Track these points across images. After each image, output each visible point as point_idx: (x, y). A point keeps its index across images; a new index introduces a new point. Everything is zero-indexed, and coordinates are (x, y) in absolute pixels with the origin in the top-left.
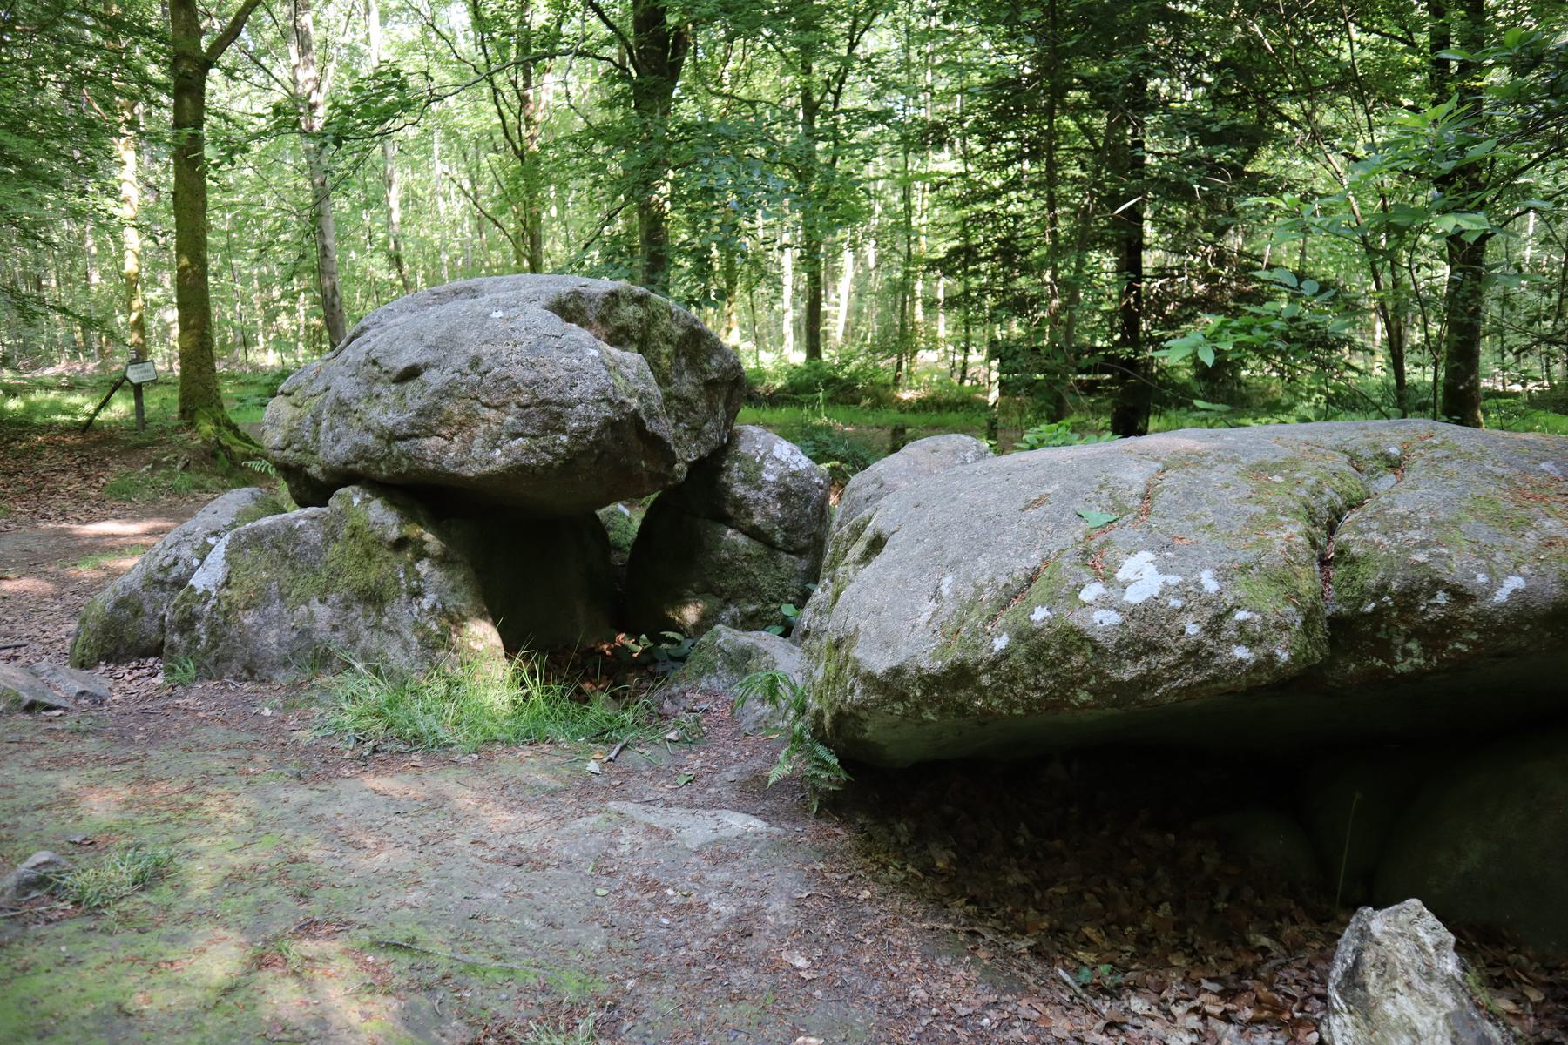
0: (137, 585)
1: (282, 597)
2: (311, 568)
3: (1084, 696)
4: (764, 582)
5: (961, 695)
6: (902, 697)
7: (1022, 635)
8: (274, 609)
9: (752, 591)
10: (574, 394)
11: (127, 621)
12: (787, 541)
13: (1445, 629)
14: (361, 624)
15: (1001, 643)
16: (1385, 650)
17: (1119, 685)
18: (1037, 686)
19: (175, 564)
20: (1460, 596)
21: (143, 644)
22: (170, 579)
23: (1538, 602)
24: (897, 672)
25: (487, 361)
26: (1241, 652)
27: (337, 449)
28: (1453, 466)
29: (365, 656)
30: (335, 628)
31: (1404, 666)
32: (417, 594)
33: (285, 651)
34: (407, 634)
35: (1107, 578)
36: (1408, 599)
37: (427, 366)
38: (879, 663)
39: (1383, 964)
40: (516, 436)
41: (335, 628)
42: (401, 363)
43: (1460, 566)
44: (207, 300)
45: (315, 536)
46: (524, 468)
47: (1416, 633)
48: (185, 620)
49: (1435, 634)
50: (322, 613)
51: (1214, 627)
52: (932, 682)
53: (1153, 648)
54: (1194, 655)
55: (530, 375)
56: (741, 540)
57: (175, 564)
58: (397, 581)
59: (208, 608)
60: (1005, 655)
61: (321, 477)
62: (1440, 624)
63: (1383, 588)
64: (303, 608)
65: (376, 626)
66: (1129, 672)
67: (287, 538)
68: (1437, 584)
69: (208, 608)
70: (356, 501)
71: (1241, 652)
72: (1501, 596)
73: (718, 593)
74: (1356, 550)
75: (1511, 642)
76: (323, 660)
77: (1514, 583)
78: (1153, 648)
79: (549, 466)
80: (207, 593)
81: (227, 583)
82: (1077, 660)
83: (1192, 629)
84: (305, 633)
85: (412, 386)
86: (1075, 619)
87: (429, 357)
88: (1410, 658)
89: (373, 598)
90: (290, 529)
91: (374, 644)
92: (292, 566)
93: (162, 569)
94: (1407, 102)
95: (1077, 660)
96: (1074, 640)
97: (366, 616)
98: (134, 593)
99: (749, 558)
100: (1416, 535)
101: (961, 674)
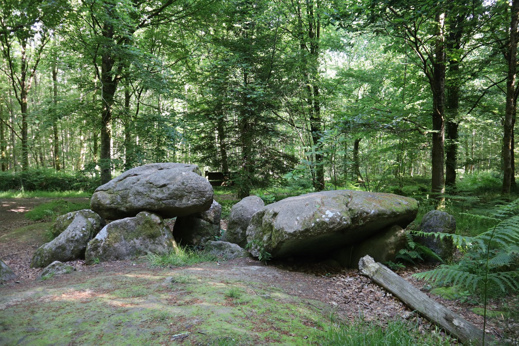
0: (64, 242)
1: (125, 239)
2: (132, 231)
3: (325, 231)
4: (210, 231)
5: (306, 234)
6: (295, 236)
7: (316, 223)
8: (123, 242)
9: (208, 234)
10: (207, 189)
11: (60, 252)
12: (215, 222)
13: (366, 218)
14: (149, 243)
15: (313, 225)
16: (358, 222)
17: (330, 228)
18: (319, 230)
19: (76, 236)
20: (367, 213)
21: (65, 258)
22: (75, 240)
23: (376, 213)
24: (295, 232)
25: (186, 183)
26: (345, 222)
27: (139, 203)
28: (358, 196)
29: (150, 250)
30: (141, 245)
31: (361, 224)
32: (164, 235)
33: (128, 252)
34: (164, 244)
35: (325, 214)
36: (361, 214)
37: (168, 184)
38: (291, 231)
39: (367, 262)
40: (194, 198)
41: (141, 245)
42: (162, 183)
43: (366, 209)
44: (433, 172)
45: (133, 224)
46: (196, 205)
47: (362, 219)
48: (95, 248)
49: (364, 219)
50: (138, 242)
51: (341, 219)
52: (301, 232)
53: (334, 223)
54: (339, 223)
55: (196, 186)
56: (205, 222)
57: (76, 236)
58: (160, 232)
59: (102, 244)
60: (314, 226)
61: (125, 210)
62: (365, 217)
63: (358, 213)
64: (132, 241)
65: (153, 243)
66: (331, 227)
67: (125, 225)
68: (364, 212)
69: (102, 244)
70: (147, 215)
71: (345, 222)
72: (372, 213)
73: (201, 234)
74: (352, 209)
75: (374, 219)
76: (139, 252)
77: (373, 211)
78: (334, 223)
79: (201, 204)
80: (102, 241)
81: (108, 237)
82: (324, 226)
83: (338, 220)
84: (134, 247)
85: (164, 189)
86: (323, 220)
87: (168, 182)
88: (361, 223)
89: (153, 237)
90: (126, 222)
91: (153, 247)
92: (127, 232)
93: (72, 237)
94: (459, 167)
95: (324, 226)
96: (324, 223)
97: (150, 241)
98: (63, 245)
99: (207, 226)
100: (360, 206)
101: (307, 230)
